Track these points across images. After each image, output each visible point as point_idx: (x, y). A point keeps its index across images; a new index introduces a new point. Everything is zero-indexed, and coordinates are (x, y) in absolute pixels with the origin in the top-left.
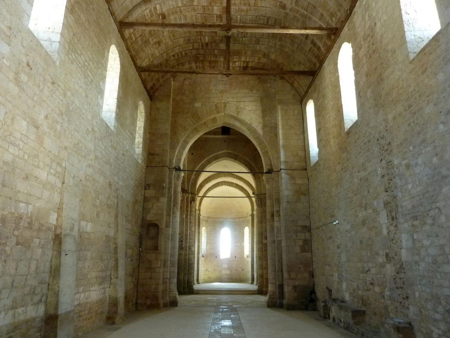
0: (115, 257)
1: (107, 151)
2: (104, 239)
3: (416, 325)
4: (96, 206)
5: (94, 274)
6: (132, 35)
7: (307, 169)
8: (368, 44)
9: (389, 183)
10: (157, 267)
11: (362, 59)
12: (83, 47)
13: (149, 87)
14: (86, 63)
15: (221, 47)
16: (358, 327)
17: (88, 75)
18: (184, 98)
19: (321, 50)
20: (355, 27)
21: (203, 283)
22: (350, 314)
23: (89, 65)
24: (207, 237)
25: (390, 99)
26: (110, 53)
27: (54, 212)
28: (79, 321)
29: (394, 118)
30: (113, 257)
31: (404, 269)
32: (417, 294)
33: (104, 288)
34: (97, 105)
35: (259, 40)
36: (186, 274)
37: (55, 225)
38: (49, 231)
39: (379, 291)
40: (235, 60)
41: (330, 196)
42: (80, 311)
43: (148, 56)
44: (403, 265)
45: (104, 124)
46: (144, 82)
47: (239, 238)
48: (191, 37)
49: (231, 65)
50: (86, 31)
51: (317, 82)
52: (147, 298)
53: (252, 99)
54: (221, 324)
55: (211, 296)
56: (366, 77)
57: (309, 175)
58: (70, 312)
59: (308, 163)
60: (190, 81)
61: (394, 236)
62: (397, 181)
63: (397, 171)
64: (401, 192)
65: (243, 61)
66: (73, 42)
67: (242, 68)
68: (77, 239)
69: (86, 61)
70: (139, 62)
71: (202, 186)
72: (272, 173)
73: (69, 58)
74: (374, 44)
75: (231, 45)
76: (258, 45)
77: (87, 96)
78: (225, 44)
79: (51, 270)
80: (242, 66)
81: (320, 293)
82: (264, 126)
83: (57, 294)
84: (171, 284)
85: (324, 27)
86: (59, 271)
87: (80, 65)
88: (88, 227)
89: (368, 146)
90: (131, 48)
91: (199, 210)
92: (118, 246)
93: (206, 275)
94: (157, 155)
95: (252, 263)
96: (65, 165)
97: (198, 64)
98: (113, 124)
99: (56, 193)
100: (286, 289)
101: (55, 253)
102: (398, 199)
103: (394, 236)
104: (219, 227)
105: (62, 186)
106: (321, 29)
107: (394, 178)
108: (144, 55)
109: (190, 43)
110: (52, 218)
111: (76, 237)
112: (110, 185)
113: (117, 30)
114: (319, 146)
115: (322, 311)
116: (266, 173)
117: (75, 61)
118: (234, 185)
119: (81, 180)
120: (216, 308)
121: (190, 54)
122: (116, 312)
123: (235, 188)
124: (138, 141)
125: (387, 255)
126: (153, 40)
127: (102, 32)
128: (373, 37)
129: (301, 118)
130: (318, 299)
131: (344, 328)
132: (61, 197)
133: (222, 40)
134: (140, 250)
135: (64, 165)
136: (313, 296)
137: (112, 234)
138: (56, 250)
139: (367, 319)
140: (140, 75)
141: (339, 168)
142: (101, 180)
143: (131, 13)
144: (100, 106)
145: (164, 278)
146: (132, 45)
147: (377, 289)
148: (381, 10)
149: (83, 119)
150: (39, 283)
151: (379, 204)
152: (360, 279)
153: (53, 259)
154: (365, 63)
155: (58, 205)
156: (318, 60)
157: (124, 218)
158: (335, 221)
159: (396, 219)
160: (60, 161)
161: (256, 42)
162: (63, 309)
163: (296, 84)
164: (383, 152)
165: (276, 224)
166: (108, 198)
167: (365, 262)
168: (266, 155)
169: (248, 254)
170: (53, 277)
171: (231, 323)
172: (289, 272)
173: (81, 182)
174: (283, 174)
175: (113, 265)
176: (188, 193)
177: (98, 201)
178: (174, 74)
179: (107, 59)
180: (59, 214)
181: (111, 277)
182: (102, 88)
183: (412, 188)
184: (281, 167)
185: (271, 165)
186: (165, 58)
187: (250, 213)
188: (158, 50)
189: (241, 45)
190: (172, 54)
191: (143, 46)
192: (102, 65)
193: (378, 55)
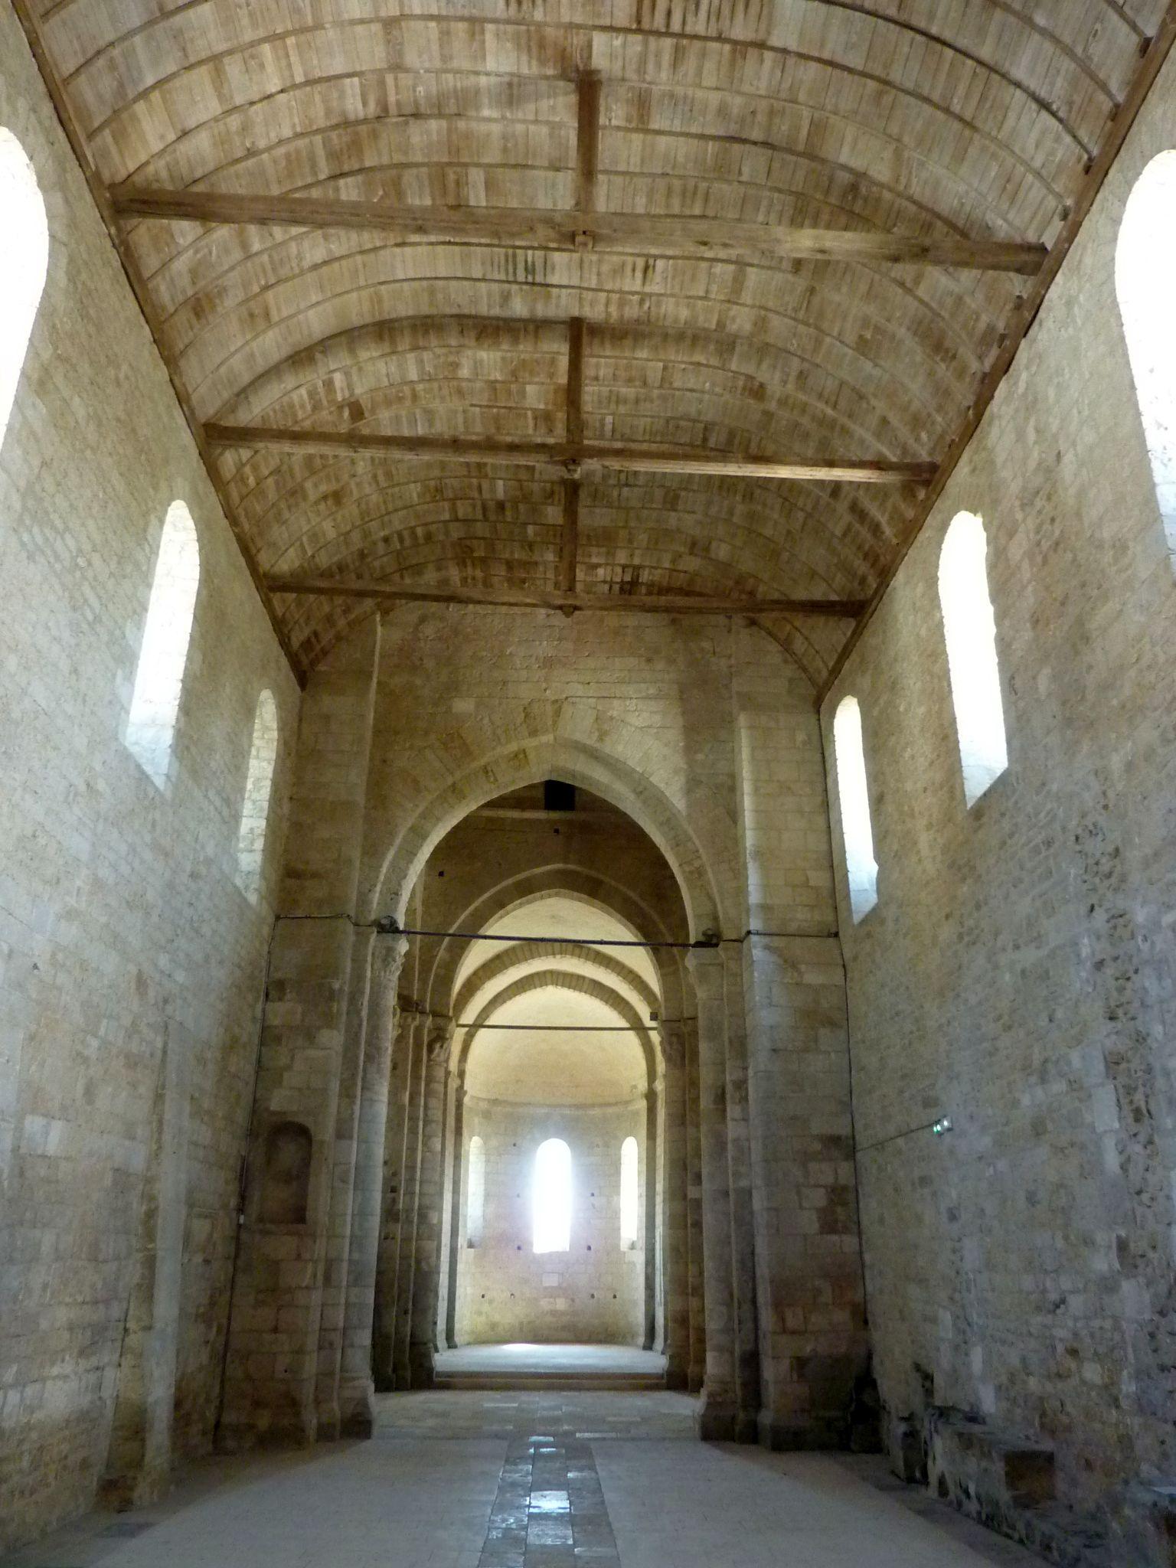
2: (108, 1181)
4: (86, 1060)
5: (62, 1315)
6: (247, 470)
7: (841, 934)
8: (1038, 521)
9: (1121, 990)
10: (300, 1288)
11: (1019, 568)
12: (71, 505)
13: (296, 640)
17: (86, 601)
18: (418, 682)
21: (469, 1344)
22: (999, 1468)
24: (487, 1174)
29: (1130, 767)
34: (110, 702)
35: (677, 497)
36: (406, 1312)
40: (594, 560)
41: (918, 1030)
43: (299, 539)
46: (280, 625)
50: (88, 452)
51: (870, 639)
52: (257, 1404)
53: (651, 691)
54: (529, 1506)
55: (497, 1395)
57: (847, 955)
59: (842, 915)
63: (1145, 947)
64: (1163, 1023)
67: (616, 588)
69: (80, 551)
70: (265, 560)
71: (472, 986)
72: (716, 945)
73: (23, 544)
74: (1058, 521)
75: (582, 512)
78: (561, 508)
80: (619, 580)
82: (692, 784)
85: (894, 459)
87: (58, 566)
89: (1047, 857)
91: (461, 1074)
92: (157, 1208)
93: (480, 1313)
94: (315, 875)
95: (650, 1270)
98: (164, 769)
100: (770, 1371)
107: (1136, 971)
108: (286, 535)
112: (141, 983)
114: (878, 856)
116: (699, 944)
117: (43, 552)
118: (585, 987)
119: (35, 967)
121: (441, 537)
123: (591, 995)
125: (1122, 1246)
126: (316, 486)
129: (818, 756)
130: (884, 1408)
131: (979, 1521)
133: (552, 493)
140: (267, 603)
141: (947, 932)
142: (110, 964)
143: (247, 398)
144: (119, 707)
145: (325, 1330)
147: (1092, 1373)
148: (1075, 411)
149: (56, 748)
152: (1030, 1334)
154: (1029, 582)
156: (873, 565)
158: (938, 1122)
161: (665, 502)
163: (799, 645)
166: (132, 1031)
168: (700, 883)
169: (635, 1239)
171: (566, 1504)
172: (778, 1305)
174: (757, 950)
175: (136, 1279)
176: (423, 1013)
177: (95, 1043)
178: (387, 602)
182: (131, 643)
185: (716, 918)
187: (642, 1085)
188: (334, 520)
190: (382, 534)
192: (137, 565)
193: (1069, 556)
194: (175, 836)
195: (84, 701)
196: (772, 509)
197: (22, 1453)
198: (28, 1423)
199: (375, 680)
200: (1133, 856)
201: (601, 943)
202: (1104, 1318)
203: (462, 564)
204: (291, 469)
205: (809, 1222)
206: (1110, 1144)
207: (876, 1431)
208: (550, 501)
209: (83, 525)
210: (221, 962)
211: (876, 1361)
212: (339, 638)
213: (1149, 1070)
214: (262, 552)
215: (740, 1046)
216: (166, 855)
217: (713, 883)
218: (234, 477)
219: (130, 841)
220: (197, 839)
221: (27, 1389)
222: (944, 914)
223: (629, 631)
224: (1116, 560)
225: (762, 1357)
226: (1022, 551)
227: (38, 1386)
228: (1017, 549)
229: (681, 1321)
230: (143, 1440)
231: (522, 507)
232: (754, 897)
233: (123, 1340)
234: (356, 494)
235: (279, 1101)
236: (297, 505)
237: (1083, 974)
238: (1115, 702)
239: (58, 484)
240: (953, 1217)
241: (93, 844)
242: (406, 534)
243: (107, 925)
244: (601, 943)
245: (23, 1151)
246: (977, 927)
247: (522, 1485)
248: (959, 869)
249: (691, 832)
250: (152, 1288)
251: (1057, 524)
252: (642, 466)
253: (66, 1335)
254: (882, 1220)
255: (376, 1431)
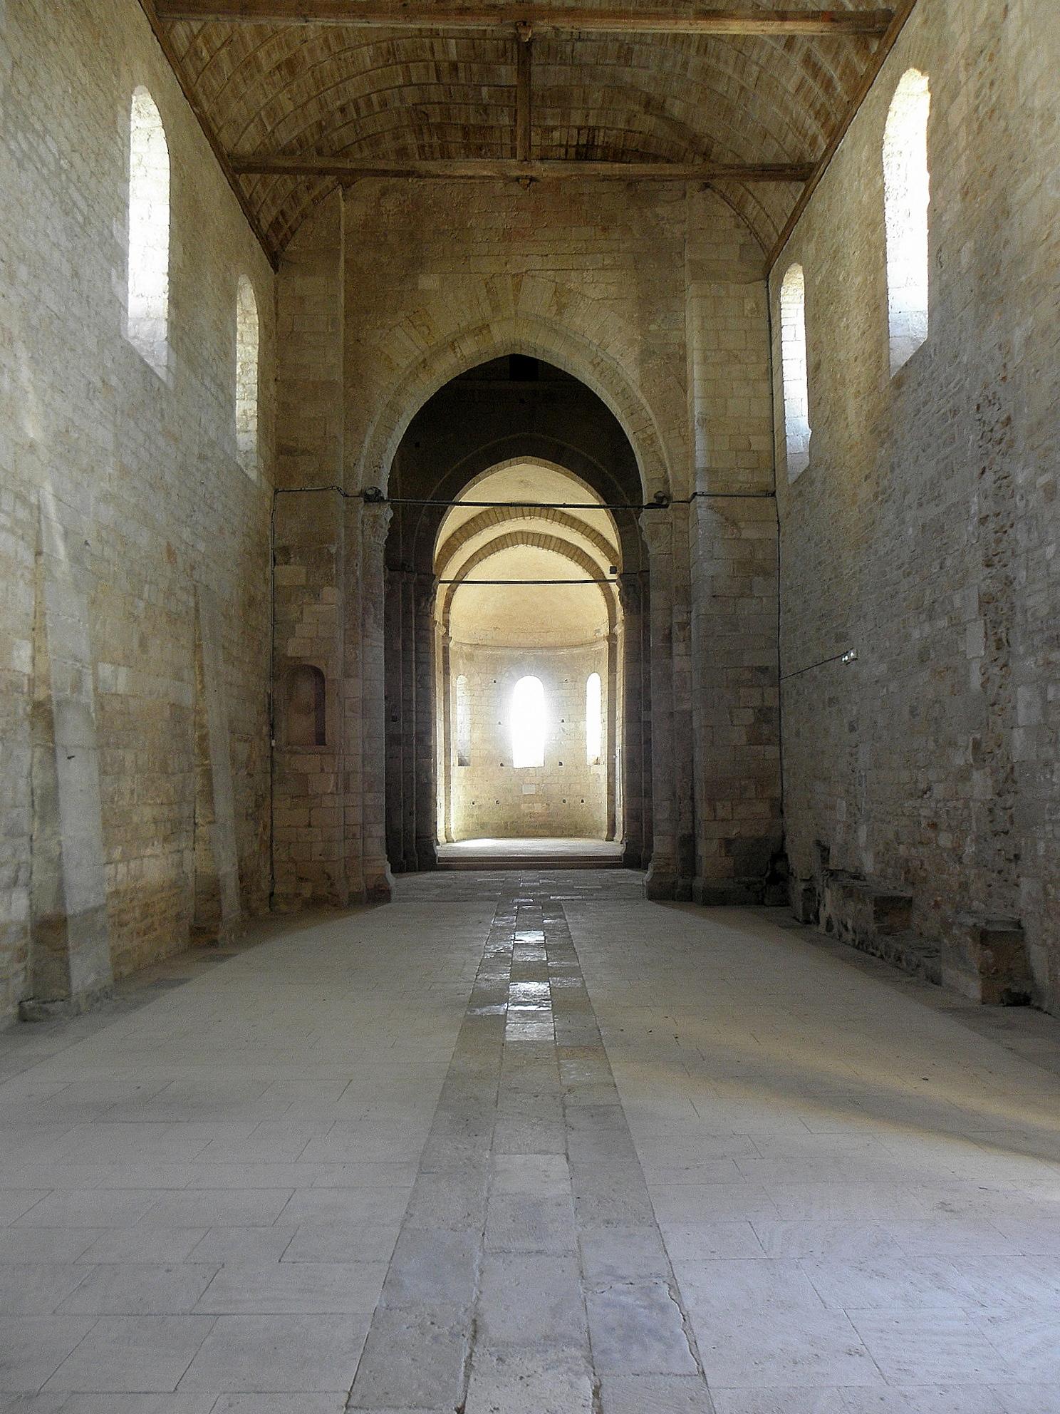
0: (203, 765)
1: (153, 450)
2: (167, 713)
3: (1031, 926)
4: (136, 618)
5: (148, 813)
6: (200, 41)
7: (777, 494)
9: (998, 541)
10: (325, 793)
12: (46, 106)
13: (265, 225)
14: (62, 162)
15: (500, 76)
16: (888, 939)
17: (75, 204)
19: (835, 89)
20: (945, 13)
22: (870, 908)
23: (72, 166)
25: (1023, 278)
26: (134, 115)
27: (25, 638)
28: (119, 936)
29: (1028, 341)
30: (197, 766)
31: (1015, 782)
32: (1041, 846)
33: (179, 851)
34: (110, 302)
35: (630, 51)
36: (411, 814)
37: (29, 675)
38: (15, 694)
39: (949, 845)
40: (550, 123)
41: (836, 577)
42: (121, 911)
43: (258, 114)
44: (1015, 773)
45: (137, 362)
46: (248, 207)
47: (573, 705)
48: (399, 42)
49: (536, 139)
50: (51, 45)
51: (818, 204)
54: (514, 940)
56: (963, 199)
58: (96, 910)
59: (779, 475)
60: (402, 199)
61: (998, 694)
62: (1020, 535)
63: (1021, 504)
64: (1027, 568)
65: (576, 127)
66: (14, 91)
67: (572, 151)
68: (94, 714)
69: (61, 153)
70: (225, 137)
71: (452, 547)
72: (666, 506)
73: (12, 152)
74: (997, 84)
75: (535, 69)
76: (627, 69)
77: (76, 274)
79: (33, 801)
80: (575, 143)
81: (801, 860)
82: (646, 354)
83: (57, 863)
84: (369, 840)
86: (56, 802)
87: (45, 171)
88: (118, 679)
89: (952, 425)
90: (201, 90)
91: (446, 624)
92: (207, 734)
94: (304, 452)
96: (39, 501)
97: (426, 137)
98: (164, 361)
99: (21, 583)
100: (703, 849)
101: (38, 753)
102: (1018, 588)
103: (998, 694)
104: (507, 675)
105: (36, 562)
106: (837, 17)
107: (1012, 526)
108: (244, 112)
109: (397, 63)
110: (19, 657)
111: (92, 709)
112: (171, 553)
113: (146, 27)
115: (801, 904)
116: (651, 506)
117: (30, 159)
119: (86, 543)
120: (504, 899)
121: (397, 104)
122: (219, 916)
124: (242, 409)
125: (977, 745)
127: (101, 42)
128: (995, 60)
129: (765, 326)
130: (792, 874)
131: (854, 946)
132: (36, 596)
134: (273, 744)
135: (33, 499)
136: (779, 866)
137: (188, 700)
138: (42, 746)
139: (916, 918)
140: (234, 185)
141: (865, 491)
142: (144, 539)
144: (118, 305)
146: (201, 77)
147: (945, 840)
149: (72, 350)
150: (6, 835)
151: (966, 602)
152: (903, 814)
153: (35, 769)
154: (964, 151)
155: (32, 617)
157: (220, 652)
158: (845, 654)
159: (1006, 644)
160: (22, 488)
161: (619, 57)
162: (76, 903)
163: (751, 209)
164: (990, 445)
165: (679, 663)
166: (170, 594)
167: (919, 768)
170: (40, 818)
172: (711, 801)
173: (87, 547)
174: (701, 510)
175: (198, 788)
177: (142, 604)
178: (347, 179)
179: (126, 141)
180: (37, 644)
181: (197, 821)
182: (119, 241)
183: (1054, 558)
184: (695, 488)
185: (666, 482)
186: (317, 117)
187: (605, 630)
188: (290, 91)
189: (569, 68)
190: (338, 103)
191: (238, 78)
192: (113, 161)
193: (1002, 124)
194: (181, 422)
195: (88, 303)
196: (726, 62)
197: (134, 907)
198: (135, 887)
199: (342, 258)
200: (1021, 424)
201: (565, 506)
202: (957, 800)
203: (419, 132)
204: (242, 37)
205: (738, 736)
206: (975, 668)
207: (784, 891)
208: (502, 60)
209: (60, 125)
210: (233, 533)
211: (788, 839)
212: (304, 216)
213: (1012, 608)
214: (224, 130)
215: (685, 594)
216: (176, 440)
217: (664, 448)
218: (188, 51)
219: (145, 430)
220: (200, 425)
221: (131, 864)
222: (863, 476)
223: (586, 198)
224: (1043, 130)
225: (698, 840)
226: (960, 117)
227: (138, 862)
228: (957, 114)
229: (634, 816)
230: (219, 901)
231: (475, 67)
232: (701, 461)
233: (194, 832)
234: (309, 62)
235: (293, 648)
236: (252, 76)
237: (970, 528)
238: (1023, 278)
239: (31, 84)
240: (852, 729)
241: (116, 435)
242: (362, 103)
243: (136, 505)
244: (565, 506)
245: (100, 690)
246: (890, 488)
247: (510, 928)
248: (879, 435)
249: (644, 401)
250: (212, 794)
251: (996, 87)
252: (593, 27)
253: (153, 827)
254: (798, 734)
255: (393, 897)
